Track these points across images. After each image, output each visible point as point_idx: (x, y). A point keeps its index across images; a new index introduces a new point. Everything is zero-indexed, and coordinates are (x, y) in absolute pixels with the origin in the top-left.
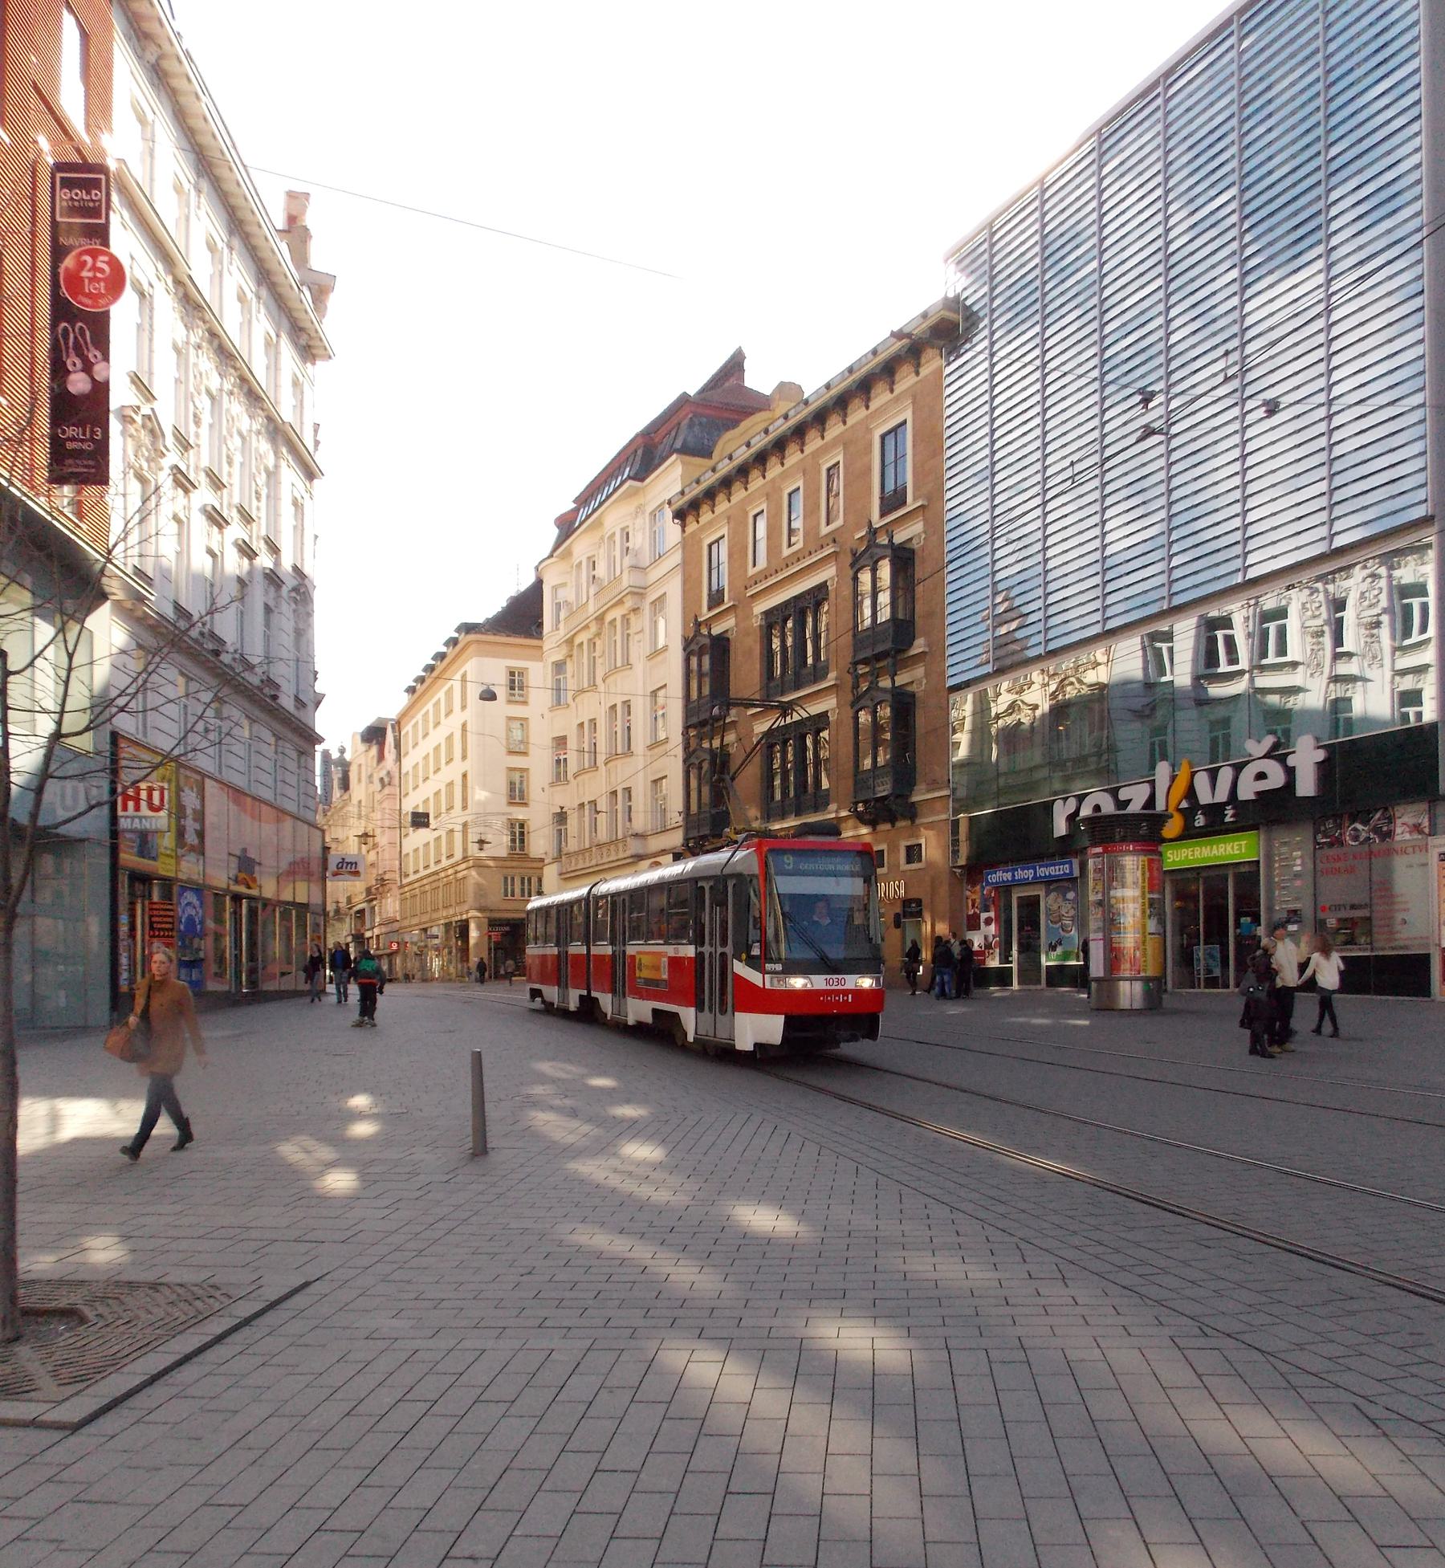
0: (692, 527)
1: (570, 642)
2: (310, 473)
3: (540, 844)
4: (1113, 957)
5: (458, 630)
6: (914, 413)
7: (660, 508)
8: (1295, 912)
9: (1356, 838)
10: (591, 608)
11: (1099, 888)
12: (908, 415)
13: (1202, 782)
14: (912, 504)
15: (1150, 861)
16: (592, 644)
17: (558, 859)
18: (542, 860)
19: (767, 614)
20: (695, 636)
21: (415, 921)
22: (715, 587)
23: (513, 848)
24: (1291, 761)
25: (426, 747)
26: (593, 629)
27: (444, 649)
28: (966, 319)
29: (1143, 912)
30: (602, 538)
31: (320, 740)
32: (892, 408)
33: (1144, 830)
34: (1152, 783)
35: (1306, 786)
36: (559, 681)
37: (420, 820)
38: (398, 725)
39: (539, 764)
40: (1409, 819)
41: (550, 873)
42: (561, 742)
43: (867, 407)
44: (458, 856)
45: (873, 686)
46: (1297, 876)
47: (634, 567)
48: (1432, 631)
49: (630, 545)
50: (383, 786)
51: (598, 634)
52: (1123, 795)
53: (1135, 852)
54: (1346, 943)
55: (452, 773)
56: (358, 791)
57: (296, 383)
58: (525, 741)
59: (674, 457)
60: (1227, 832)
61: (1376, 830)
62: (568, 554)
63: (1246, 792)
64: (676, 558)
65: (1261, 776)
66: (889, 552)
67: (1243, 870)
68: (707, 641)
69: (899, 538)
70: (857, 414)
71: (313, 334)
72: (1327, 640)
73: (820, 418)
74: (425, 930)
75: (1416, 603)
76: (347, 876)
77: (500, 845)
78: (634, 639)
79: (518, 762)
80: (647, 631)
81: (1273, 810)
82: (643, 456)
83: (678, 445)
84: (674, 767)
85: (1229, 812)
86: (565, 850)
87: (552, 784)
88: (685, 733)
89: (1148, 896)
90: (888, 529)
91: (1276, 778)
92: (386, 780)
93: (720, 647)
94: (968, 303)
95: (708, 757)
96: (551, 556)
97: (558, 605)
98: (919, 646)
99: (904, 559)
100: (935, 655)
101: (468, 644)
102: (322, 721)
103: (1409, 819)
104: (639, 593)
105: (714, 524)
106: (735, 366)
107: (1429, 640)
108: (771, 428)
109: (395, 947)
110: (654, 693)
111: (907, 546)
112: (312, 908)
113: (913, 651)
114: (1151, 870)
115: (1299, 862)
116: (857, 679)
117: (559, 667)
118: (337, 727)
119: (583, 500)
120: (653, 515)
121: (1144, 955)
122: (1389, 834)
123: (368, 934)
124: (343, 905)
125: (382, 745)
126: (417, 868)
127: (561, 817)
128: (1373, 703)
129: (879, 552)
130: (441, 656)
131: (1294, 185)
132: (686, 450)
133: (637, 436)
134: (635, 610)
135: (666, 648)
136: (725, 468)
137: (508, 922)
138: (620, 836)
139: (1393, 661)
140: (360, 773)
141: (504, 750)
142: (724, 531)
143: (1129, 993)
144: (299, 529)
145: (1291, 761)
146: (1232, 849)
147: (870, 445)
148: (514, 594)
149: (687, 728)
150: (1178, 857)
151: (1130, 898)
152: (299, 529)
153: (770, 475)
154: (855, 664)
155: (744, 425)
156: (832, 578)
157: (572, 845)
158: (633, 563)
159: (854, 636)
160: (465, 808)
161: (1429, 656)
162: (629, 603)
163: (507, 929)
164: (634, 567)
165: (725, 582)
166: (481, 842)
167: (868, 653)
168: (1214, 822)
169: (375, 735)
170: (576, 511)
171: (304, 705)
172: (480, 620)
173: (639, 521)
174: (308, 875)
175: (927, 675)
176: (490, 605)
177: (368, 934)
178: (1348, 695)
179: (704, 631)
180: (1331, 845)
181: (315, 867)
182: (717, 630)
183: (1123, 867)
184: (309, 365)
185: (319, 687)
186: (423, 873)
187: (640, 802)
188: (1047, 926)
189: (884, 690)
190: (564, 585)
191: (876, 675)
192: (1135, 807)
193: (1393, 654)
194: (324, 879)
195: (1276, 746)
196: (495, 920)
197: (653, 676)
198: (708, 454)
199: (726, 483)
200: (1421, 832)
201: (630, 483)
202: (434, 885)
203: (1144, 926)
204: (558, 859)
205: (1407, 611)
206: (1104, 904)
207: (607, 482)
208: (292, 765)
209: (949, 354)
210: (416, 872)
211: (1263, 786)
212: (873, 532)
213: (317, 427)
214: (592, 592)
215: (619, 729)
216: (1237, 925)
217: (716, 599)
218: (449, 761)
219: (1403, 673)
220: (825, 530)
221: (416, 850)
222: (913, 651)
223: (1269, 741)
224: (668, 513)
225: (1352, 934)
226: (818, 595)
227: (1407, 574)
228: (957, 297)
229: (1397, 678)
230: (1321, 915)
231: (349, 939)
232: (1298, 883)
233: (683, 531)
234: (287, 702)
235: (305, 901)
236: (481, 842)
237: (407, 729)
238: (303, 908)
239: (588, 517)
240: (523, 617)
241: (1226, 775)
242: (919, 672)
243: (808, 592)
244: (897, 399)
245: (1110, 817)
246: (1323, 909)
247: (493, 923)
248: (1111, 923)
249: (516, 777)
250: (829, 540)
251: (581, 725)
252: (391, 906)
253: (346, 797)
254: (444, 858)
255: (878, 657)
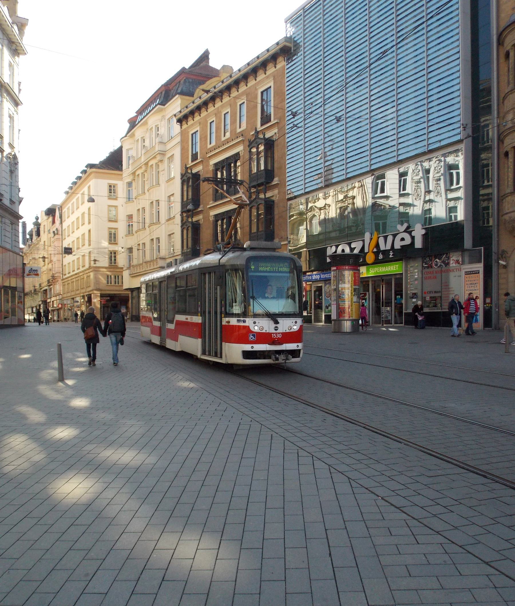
0: (185, 126)
1: (134, 173)
2: (16, 103)
3: (122, 260)
4: (341, 311)
5: (87, 167)
6: (274, 83)
7: (171, 117)
8: (415, 294)
9: (436, 265)
10: (143, 159)
11: (335, 283)
12: (271, 84)
13: (381, 241)
14: (273, 121)
15: (355, 273)
16: (143, 175)
17: (129, 268)
18: (122, 268)
19: (216, 165)
20: (185, 173)
21: (69, 295)
22: (194, 152)
23: (111, 263)
24: (413, 234)
25: (73, 218)
26: (144, 168)
27: (81, 175)
28: (295, 46)
29: (352, 293)
30: (147, 129)
31: (21, 218)
32: (264, 81)
33: (356, 261)
34: (363, 241)
35: (418, 244)
36: (129, 190)
37: (68, 251)
38: (61, 208)
39: (121, 227)
40: (454, 258)
41: (126, 274)
42: (130, 217)
43: (256, 80)
44: (87, 266)
45: (257, 197)
46: (416, 279)
47: (161, 143)
48: (462, 183)
49: (159, 132)
50: (55, 235)
51: (146, 171)
52: (353, 246)
53: (348, 269)
54: (434, 307)
55: (84, 229)
56: (44, 237)
57: (10, 65)
58: (116, 215)
59: (177, 96)
60: (391, 261)
61: (443, 262)
62: (133, 135)
63: (397, 246)
64: (178, 139)
65: (403, 239)
66: (263, 141)
67: (398, 277)
68: (190, 176)
69: (267, 136)
70: (252, 82)
71: (18, 44)
72: (422, 185)
73: (236, 83)
74: (73, 299)
75: (454, 172)
76: (34, 276)
77: (104, 262)
78: (161, 173)
79: (113, 225)
80: (166, 169)
81: (406, 254)
82: (164, 95)
83: (179, 91)
84: (176, 227)
85: (391, 253)
86: (132, 264)
87: (126, 236)
88: (182, 215)
89: (353, 287)
90: (263, 132)
91: (408, 241)
92: (56, 232)
93: (196, 177)
94: (295, 39)
95: (191, 225)
96: (126, 136)
97: (129, 157)
98: (276, 181)
99: (270, 144)
100: (282, 184)
101: (91, 173)
102: (22, 210)
103: (454, 258)
104: (163, 153)
105: (194, 125)
106: (205, 57)
107: (460, 188)
108: (217, 86)
109: (60, 306)
110: (169, 197)
111: (272, 139)
112: (18, 289)
113: (273, 183)
114: (354, 277)
115: (417, 274)
116: (251, 194)
117: (130, 184)
118: (30, 211)
119: (140, 112)
120: (169, 120)
121: (352, 310)
122: (447, 264)
123: (49, 301)
124: (37, 287)
125: (54, 217)
126: (69, 272)
127: (130, 250)
128: (439, 211)
129: (260, 141)
130: (79, 178)
131: (386, 18)
132: (182, 93)
133: (162, 85)
134: (161, 161)
135: (174, 178)
136: (198, 102)
137: (109, 295)
138: (155, 258)
139: (425, 197)
140: (44, 229)
141: (106, 219)
142: (198, 129)
143: (347, 326)
144: (12, 127)
145: (413, 234)
146: (393, 268)
147: (257, 95)
148: (112, 151)
149: (182, 212)
150: (365, 272)
151: (347, 287)
152: (12, 127)
153: (217, 106)
154: (250, 188)
155: (208, 82)
156: (241, 151)
157: (135, 262)
158: (160, 140)
159: (250, 176)
160: (90, 245)
161: (460, 193)
162: (159, 158)
163: (109, 298)
164: (161, 143)
165: (198, 150)
166: (95, 261)
167: (255, 183)
168: (383, 257)
169: (51, 212)
170: (136, 117)
171: (14, 203)
172: (97, 162)
173: (163, 122)
174: (17, 275)
175: (279, 193)
176: (101, 155)
177: (49, 301)
178: (407, 211)
179: (189, 171)
180: (428, 267)
181: (20, 272)
182: (194, 171)
183: (344, 275)
184: (16, 57)
185: (21, 195)
186: (72, 274)
187: (163, 244)
188: (325, 299)
189: (261, 199)
190: (131, 149)
191: (258, 192)
192: (356, 251)
193: (425, 194)
194: (23, 277)
195: (408, 227)
196: (104, 294)
197: (169, 191)
198: (192, 95)
199: (199, 108)
200: (459, 263)
201: (159, 106)
202: (77, 279)
203: (352, 299)
204: (129, 268)
205: (451, 175)
206: (336, 290)
207: (149, 105)
208: (9, 228)
209: (288, 59)
210: (69, 273)
211: (404, 243)
212: (257, 133)
213: (20, 84)
214: (143, 153)
215: (154, 212)
216: (396, 299)
217: (195, 157)
218: (83, 224)
219: (450, 200)
220: (239, 130)
221: (69, 264)
222: (273, 183)
223: (405, 225)
224: (175, 120)
225: (435, 303)
226: (236, 157)
227: (450, 160)
228: (291, 37)
229: (448, 202)
230: (424, 295)
231: (41, 303)
232: (416, 282)
233: (181, 128)
234: (6, 202)
235: (15, 286)
236: (95, 261)
237: (65, 210)
238: (14, 289)
239: (142, 120)
240: (114, 162)
241: (390, 239)
242: (276, 191)
243: (232, 156)
244: (267, 77)
245: (348, 255)
246: (425, 293)
247: (102, 296)
248: (339, 297)
249: (113, 231)
250: (241, 135)
251: (139, 210)
252: (58, 288)
253: (38, 239)
254: (81, 267)
255: (259, 185)
